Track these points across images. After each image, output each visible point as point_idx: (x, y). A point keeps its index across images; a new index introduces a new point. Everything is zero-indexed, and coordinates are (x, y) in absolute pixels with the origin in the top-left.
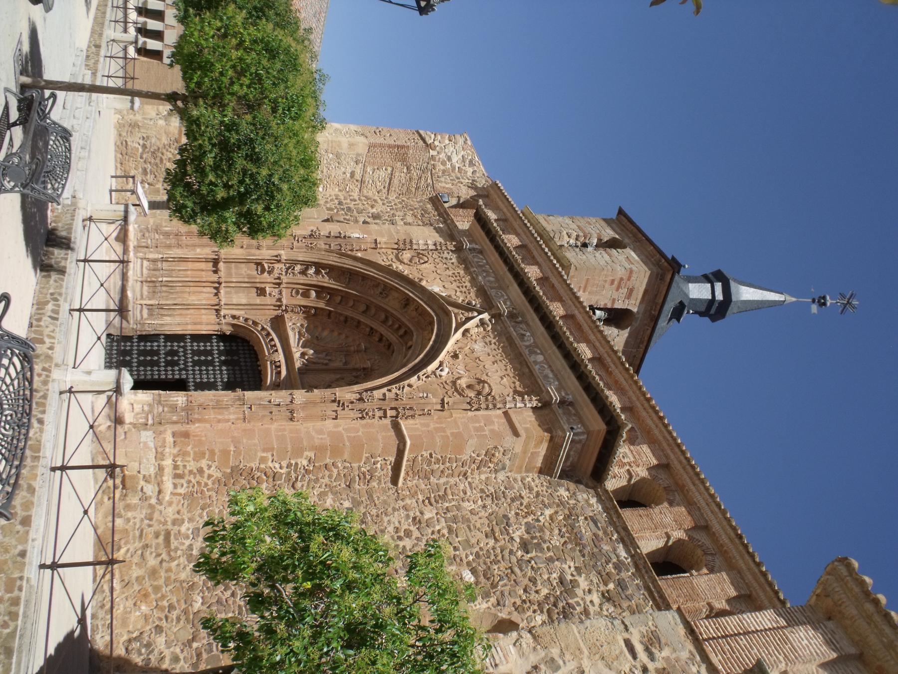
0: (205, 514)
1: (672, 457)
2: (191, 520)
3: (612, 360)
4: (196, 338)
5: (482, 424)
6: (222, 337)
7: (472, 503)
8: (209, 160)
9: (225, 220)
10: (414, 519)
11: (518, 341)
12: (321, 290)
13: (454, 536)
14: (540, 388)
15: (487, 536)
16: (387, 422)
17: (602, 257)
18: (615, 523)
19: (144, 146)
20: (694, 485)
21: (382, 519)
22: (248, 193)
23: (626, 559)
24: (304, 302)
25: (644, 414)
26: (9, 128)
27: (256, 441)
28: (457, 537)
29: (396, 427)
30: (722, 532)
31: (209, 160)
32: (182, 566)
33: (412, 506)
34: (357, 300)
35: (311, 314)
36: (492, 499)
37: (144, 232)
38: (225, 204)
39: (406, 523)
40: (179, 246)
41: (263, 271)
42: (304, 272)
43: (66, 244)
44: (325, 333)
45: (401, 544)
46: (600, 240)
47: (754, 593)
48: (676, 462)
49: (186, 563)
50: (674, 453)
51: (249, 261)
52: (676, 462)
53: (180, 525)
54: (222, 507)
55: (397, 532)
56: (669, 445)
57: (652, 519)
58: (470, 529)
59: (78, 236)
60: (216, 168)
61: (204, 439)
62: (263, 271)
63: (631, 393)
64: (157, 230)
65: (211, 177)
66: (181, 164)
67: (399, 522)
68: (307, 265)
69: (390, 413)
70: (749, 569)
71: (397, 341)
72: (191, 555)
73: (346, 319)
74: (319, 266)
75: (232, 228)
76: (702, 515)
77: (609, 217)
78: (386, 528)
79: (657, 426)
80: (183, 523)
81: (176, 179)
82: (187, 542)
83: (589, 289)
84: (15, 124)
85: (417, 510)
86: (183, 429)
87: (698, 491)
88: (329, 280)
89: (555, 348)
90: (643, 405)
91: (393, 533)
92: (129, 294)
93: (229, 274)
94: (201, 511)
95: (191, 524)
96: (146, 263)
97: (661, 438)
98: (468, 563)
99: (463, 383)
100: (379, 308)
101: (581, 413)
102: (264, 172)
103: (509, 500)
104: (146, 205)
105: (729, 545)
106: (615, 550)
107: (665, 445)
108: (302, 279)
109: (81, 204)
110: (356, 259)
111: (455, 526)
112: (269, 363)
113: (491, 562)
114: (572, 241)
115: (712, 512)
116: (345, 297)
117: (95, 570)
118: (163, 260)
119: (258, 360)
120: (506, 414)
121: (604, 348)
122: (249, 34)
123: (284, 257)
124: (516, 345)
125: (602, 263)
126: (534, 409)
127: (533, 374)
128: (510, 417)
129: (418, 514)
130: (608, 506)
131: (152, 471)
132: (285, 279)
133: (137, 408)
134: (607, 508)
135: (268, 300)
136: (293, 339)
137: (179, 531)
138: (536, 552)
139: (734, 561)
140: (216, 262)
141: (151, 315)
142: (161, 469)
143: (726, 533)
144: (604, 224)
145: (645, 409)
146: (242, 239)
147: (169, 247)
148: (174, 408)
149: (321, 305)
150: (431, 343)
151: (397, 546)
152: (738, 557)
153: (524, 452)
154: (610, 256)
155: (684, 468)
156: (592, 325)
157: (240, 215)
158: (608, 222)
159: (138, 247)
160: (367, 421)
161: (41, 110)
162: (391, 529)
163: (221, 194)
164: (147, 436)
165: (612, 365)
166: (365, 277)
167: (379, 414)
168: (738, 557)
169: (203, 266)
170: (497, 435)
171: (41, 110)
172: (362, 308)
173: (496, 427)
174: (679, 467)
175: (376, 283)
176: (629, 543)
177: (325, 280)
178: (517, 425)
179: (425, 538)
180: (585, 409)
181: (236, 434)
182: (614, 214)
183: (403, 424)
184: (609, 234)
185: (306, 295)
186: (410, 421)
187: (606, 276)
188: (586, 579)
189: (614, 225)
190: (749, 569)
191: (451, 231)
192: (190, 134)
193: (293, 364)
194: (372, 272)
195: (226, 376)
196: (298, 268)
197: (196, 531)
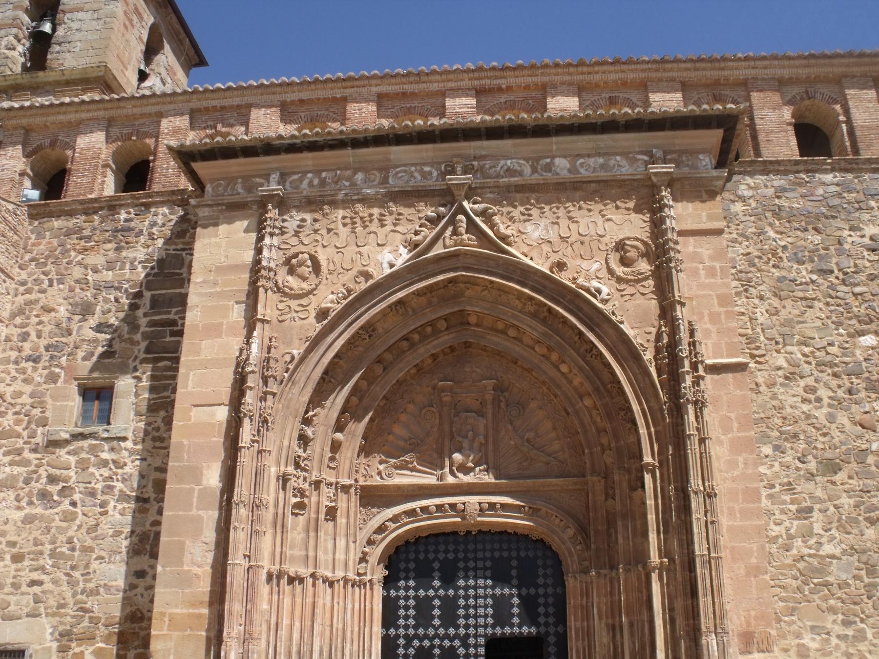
0: (786, 619)
1: (675, 74)
2: (798, 636)
3: (488, 78)
4: (389, 618)
5: (701, 266)
6: (388, 582)
7: (756, 310)
10: (786, 378)
13: (812, 341)
14: (634, 180)
15: (810, 307)
18: (785, 170)
20: (723, 69)
21: (790, 414)
23: (835, 177)
25: (597, 77)
27: (755, 547)
28: (814, 338)
30: (795, 71)
32: (872, 648)
33: (766, 376)
36: (750, 286)
39: (795, 388)
45: (826, 401)
47: (874, 74)
48: (685, 74)
49: (866, 643)
50: (671, 70)
52: (685, 74)
53: (808, 649)
54: (776, 598)
55: (810, 402)
56: (657, 70)
57: (772, 131)
58: (803, 322)
61: (753, 613)
63: (557, 78)
67: (794, 396)
70: (848, 65)
71: (454, 335)
72: (854, 637)
76: (763, 79)
78: (803, 412)
79: (623, 71)
80: (803, 645)
82: (834, 641)
85: (774, 373)
86: (736, 640)
87: (732, 69)
88: (323, 407)
89: (554, 139)
90: (582, 73)
91: (811, 406)
94: (782, 623)
95: (804, 636)
97: (643, 75)
98: (849, 335)
101: (677, 148)
103: (752, 269)
105: (813, 71)
106: (824, 184)
107: (653, 75)
111: (797, 337)
112: (479, 519)
113: (848, 312)
115: (765, 68)
119: (455, 533)
121: (462, 80)
122: (111, 469)
124: (537, 184)
127: (605, 181)
128: (687, 231)
129: (780, 373)
130: (761, 168)
134: (764, 170)
137: (817, 650)
138: (830, 262)
139: (831, 75)
143: (797, 67)
145: (589, 73)
150: (527, 291)
151: (830, 406)
152: (830, 70)
155: (696, 69)
156: (412, 79)
162: (805, 407)
165: (499, 81)
168: (830, 70)
170: (719, 255)
174: (692, 74)
176: (818, 167)
179: (815, 373)
180: (677, 141)
181: (742, 571)
188: (867, 225)
190: (848, 65)
191: (222, 204)
193: (488, 484)
195: (481, 582)
197: (817, 630)
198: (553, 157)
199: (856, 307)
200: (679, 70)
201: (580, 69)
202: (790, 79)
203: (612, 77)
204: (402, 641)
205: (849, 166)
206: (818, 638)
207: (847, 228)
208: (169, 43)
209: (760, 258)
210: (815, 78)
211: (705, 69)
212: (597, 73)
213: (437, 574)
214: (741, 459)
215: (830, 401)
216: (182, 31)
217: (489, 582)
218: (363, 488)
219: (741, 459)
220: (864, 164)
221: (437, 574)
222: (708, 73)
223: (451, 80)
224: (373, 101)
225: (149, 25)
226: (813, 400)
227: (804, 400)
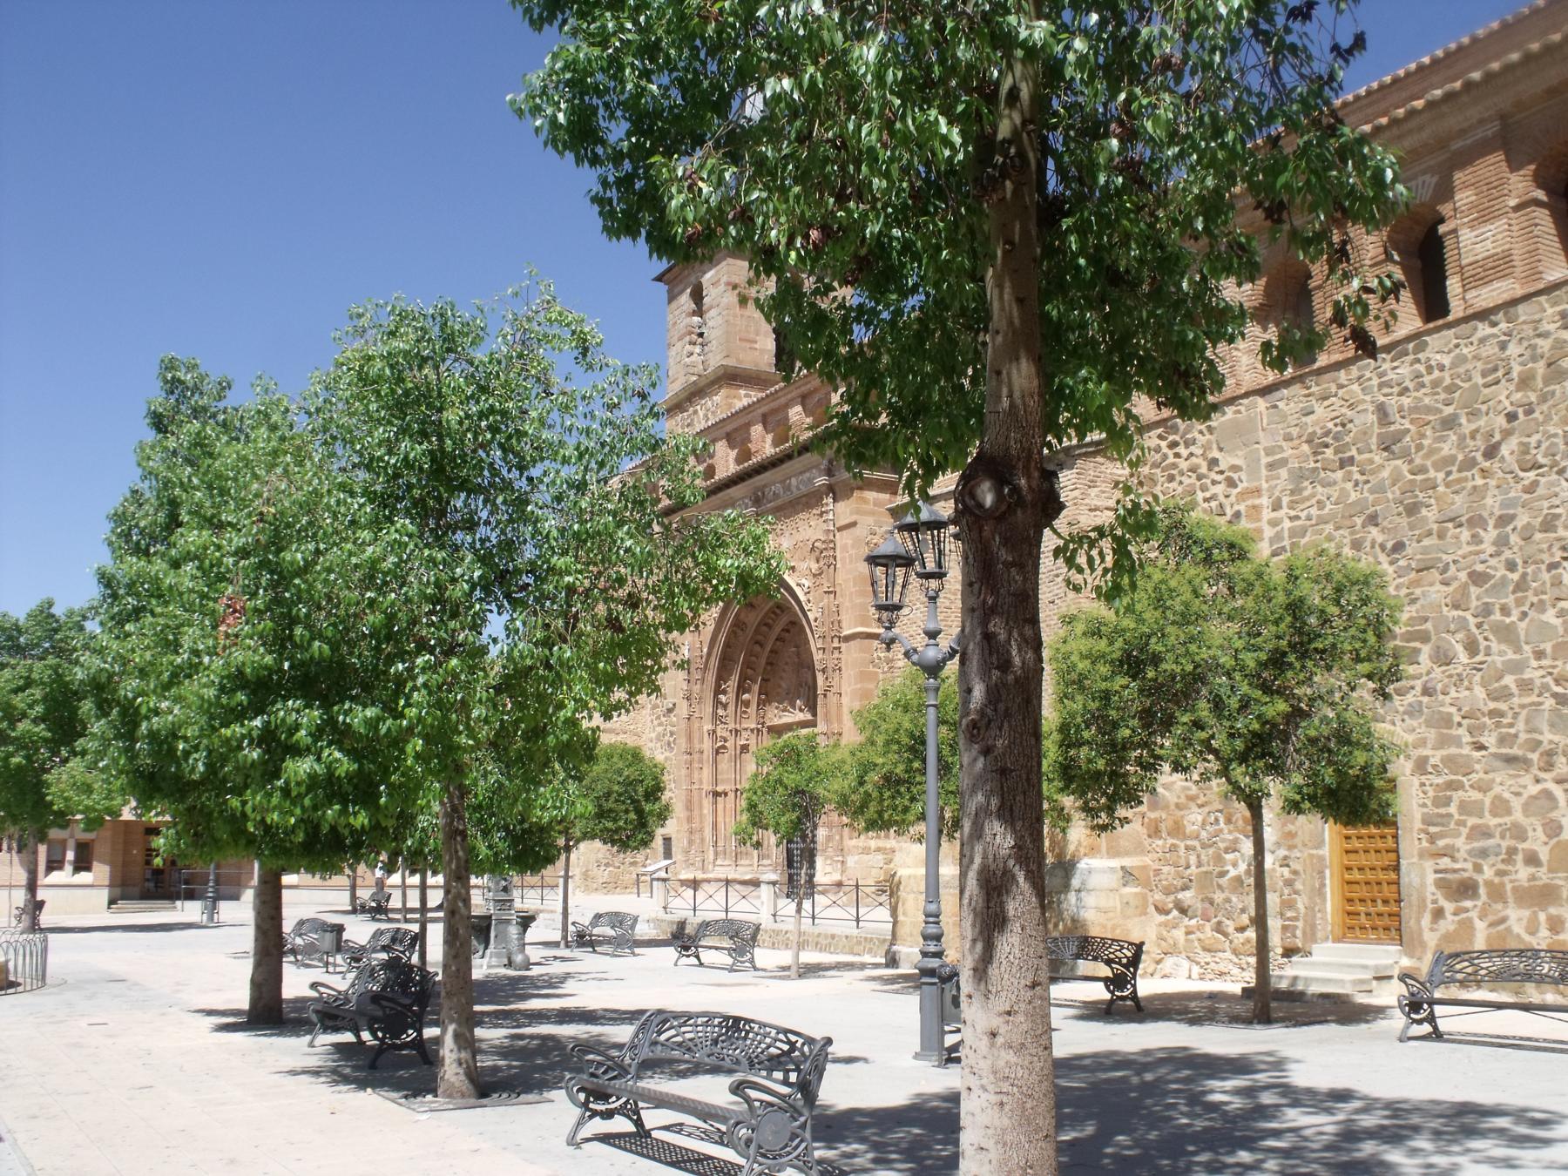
8: (610, 825)
9: (651, 811)
11: (779, 502)
12: (742, 689)
16: (843, 645)
17: (714, 318)
19: (607, 865)
22: (631, 798)
24: (754, 706)
26: (648, 1134)
29: (848, 639)
31: (610, 825)
34: (750, 654)
35: (767, 697)
37: (689, 864)
38: (640, 812)
40: (701, 830)
41: (724, 747)
42: (725, 706)
43: (682, 925)
44: (784, 685)
46: (694, 313)
51: (715, 762)
59: (679, 916)
60: (615, 820)
62: (724, 747)
64: (687, 852)
65: (621, 823)
66: (613, 842)
68: (717, 703)
69: (836, 644)
73: (769, 663)
74: (718, 691)
75: (657, 806)
77: (665, 296)
81: (624, 845)
83: (752, 336)
84: (639, 1123)
92: (748, 877)
93: (727, 781)
96: (719, 862)
99: (814, 567)
100: (757, 631)
102: (616, 788)
104: (668, 862)
108: (731, 708)
109: (653, 915)
110: (709, 654)
114: (697, 349)
116: (748, 665)
117: (404, 903)
118: (715, 845)
120: (840, 529)
123: (710, 727)
125: (720, 320)
126: (835, 500)
131: (880, 857)
132: (731, 726)
133: (828, 869)
135: (752, 742)
136: (788, 718)
140: (716, 794)
141: (768, 857)
142: (878, 850)
144: (674, 305)
146: (666, 796)
147: (703, 840)
148: (829, 838)
149: (756, 688)
153: (872, 513)
154: (711, 308)
157: (647, 800)
158: (672, 298)
159: (704, 870)
160: (843, 665)
161: (605, 1072)
163: (632, 816)
164: (851, 861)
166: (727, 645)
167: (836, 655)
169: (720, 807)
171: (605, 1072)
172: (757, 648)
173: (850, 542)
175: (733, 634)
177: (732, 684)
178: (847, 521)
182: (662, 288)
183: (846, 632)
184: (685, 300)
185: (747, 704)
186: (844, 624)
187: (735, 316)
189: (676, 290)
192: (593, 838)
194: (722, 638)
196: (721, 712)
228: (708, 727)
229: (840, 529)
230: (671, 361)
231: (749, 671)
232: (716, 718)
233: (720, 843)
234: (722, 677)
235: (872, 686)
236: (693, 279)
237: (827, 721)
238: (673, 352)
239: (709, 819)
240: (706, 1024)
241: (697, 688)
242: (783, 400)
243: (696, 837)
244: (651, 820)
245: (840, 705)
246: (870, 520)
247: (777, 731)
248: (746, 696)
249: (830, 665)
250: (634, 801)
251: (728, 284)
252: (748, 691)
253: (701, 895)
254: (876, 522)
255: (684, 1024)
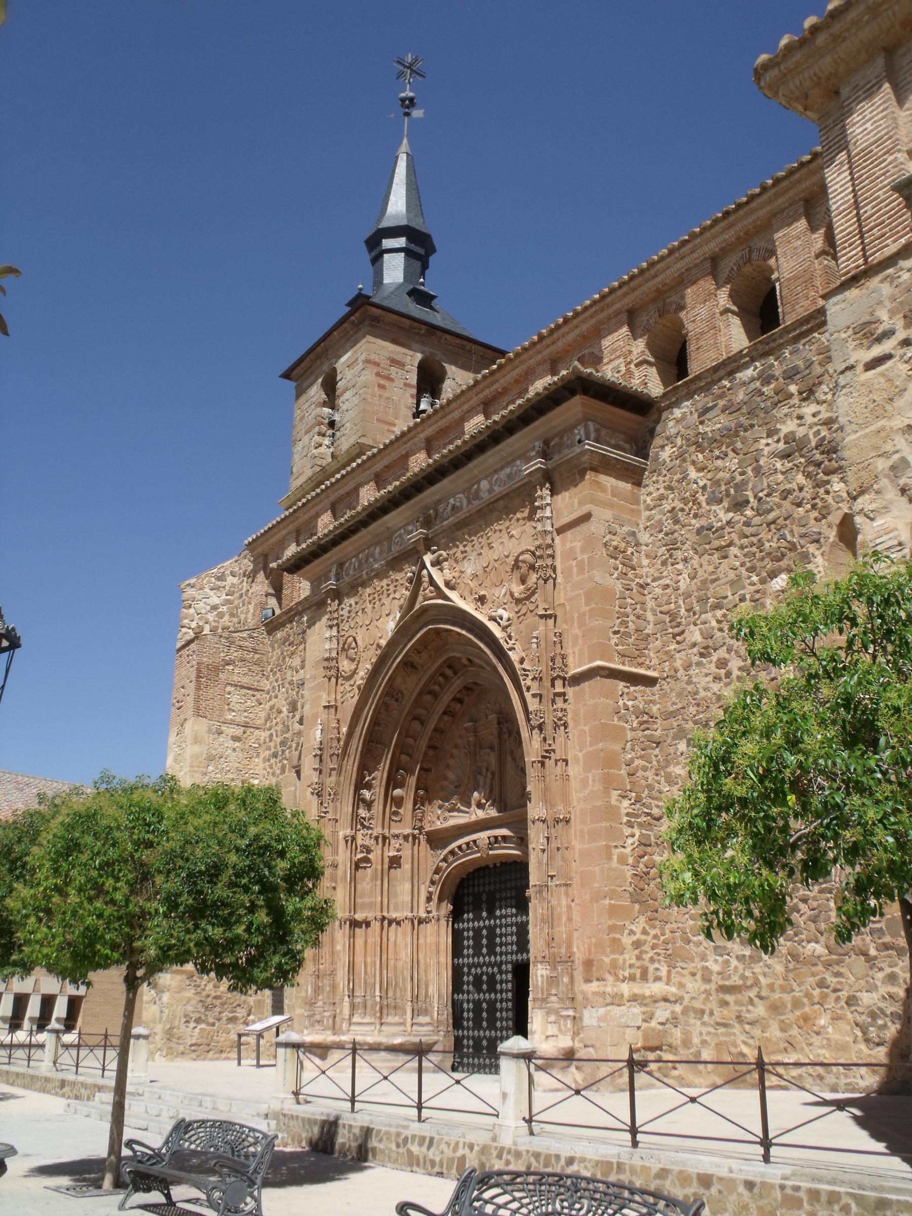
0: (695, 939)
1: (617, 306)
2: (704, 958)
3: (488, 387)
4: (457, 950)
8: (216, 933)
10: (702, 655)
11: (461, 515)
12: (392, 782)
13: (725, 601)
15: (725, 557)
16: (570, 691)
17: (347, 400)
18: (707, 384)
19: (198, 1021)
20: (656, 276)
22: (261, 881)
23: (756, 368)
24: (409, 804)
25: (560, 344)
27: (597, 869)
28: (726, 597)
29: (577, 680)
31: (216, 933)
32: (766, 970)
34: (406, 733)
37: (314, 1022)
38: (276, 911)
40: (333, 973)
41: (366, 860)
42: (369, 805)
43: (330, 1127)
44: (451, 775)
46: (325, 404)
47: (802, 195)
49: (761, 964)
51: (354, 879)
52: (626, 301)
53: (711, 972)
55: (720, 679)
56: (602, 310)
57: (702, 333)
59: (320, 1110)
60: (227, 924)
62: (366, 860)
64: (312, 1004)
66: (221, 971)
68: (359, 801)
69: (559, 688)
72: (750, 957)
74: (361, 784)
75: (309, 902)
76: (696, 265)
77: (293, 392)
79: (577, 327)
80: (707, 968)
82: (734, 962)
83: (391, 418)
90: (548, 346)
92: (398, 1041)
93: (371, 906)
96: (356, 1019)
99: (518, 589)
100: (417, 703)
101: (559, 429)
102: (233, 858)
104: (277, 1019)
106: (744, 384)
107: (601, 316)
108: (378, 807)
109: (276, 1106)
110: (350, 734)
111: (711, 600)
113: (761, 551)
114: (327, 441)
115: (693, 252)
116: (402, 748)
118: (352, 995)
119: (487, 867)
120: (560, 531)
123: (348, 832)
125: (356, 400)
126: (553, 492)
127: (506, 495)
129: (695, 650)
131: (637, 1010)
132: (378, 831)
133: (552, 1030)
134: (688, 394)
135: (406, 853)
137: (719, 973)
140: (355, 924)
142: (634, 998)
143: (721, 233)
146: (323, 889)
147: (334, 987)
148: (552, 981)
149: (412, 781)
152: (754, 217)
153: (611, 506)
157: (290, 891)
159: (335, 1030)
162: (716, 687)
163: (262, 917)
164: (590, 1017)
165: (494, 387)
167: (560, 703)
168: (754, 217)
169: (359, 942)
172: (416, 725)
173: (578, 544)
175: (383, 706)
176: (735, 364)
177: (379, 776)
181: (588, 897)
182: (291, 385)
183: (574, 670)
184: (316, 392)
185: (399, 802)
186: (570, 660)
187: (373, 395)
188: (784, 422)
189: (305, 385)
193: (492, 819)
194: (368, 712)
195: (509, 910)
196: (363, 812)
198: (478, 482)
199: (768, 541)
200: (621, 298)
201: (544, 343)
202: (722, 249)
203: (571, 337)
204: (466, 970)
205: (767, 348)
206: (720, 959)
207: (765, 435)
208: (451, 363)
209: (682, 510)
210: (746, 234)
211: (640, 286)
212: (558, 339)
213: (484, 906)
214: (590, 775)
215: (739, 673)
216: (465, 343)
217: (514, 910)
218: (428, 833)
219: (590, 775)
220: (781, 337)
221: (484, 906)
222: (645, 288)
223: (464, 403)
224: (707, 275)
225: (416, 364)
226: (723, 676)
227: (717, 678)
228: (344, 831)
229: (560, 531)
230: (296, 457)
231: (404, 757)
232: (357, 822)
233: (359, 992)
234: (366, 765)
235: (617, 747)
236: (326, 368)
237: (547, 801)
238: (299, 447)
239: (345, 958)
240: (211, 1126)
241: (331, 781)
242: (456, 414)
243: (326, 983)
244: (297, 929)
245: (566, 778)
246: (608, 514)
247: (437, 840)
248: (398, 792)
249: (549, 721)
250: (268, 888)
251: (367, 361)
252: (401, 785)
253: (33, 1051)
254: (616, 518)
255: (199, 1127)
